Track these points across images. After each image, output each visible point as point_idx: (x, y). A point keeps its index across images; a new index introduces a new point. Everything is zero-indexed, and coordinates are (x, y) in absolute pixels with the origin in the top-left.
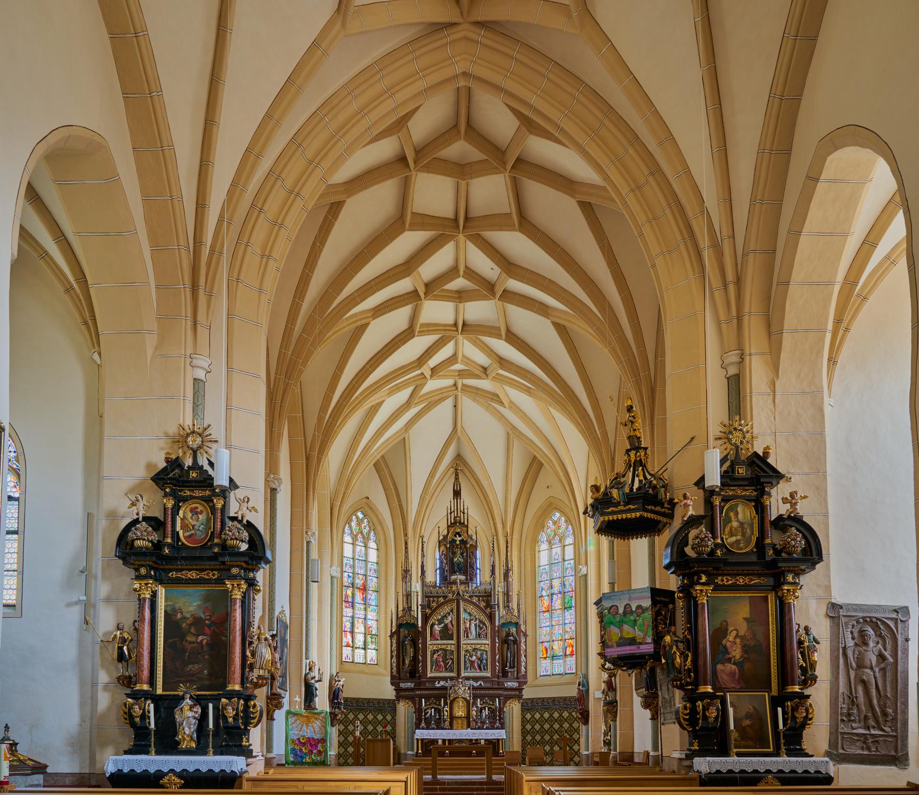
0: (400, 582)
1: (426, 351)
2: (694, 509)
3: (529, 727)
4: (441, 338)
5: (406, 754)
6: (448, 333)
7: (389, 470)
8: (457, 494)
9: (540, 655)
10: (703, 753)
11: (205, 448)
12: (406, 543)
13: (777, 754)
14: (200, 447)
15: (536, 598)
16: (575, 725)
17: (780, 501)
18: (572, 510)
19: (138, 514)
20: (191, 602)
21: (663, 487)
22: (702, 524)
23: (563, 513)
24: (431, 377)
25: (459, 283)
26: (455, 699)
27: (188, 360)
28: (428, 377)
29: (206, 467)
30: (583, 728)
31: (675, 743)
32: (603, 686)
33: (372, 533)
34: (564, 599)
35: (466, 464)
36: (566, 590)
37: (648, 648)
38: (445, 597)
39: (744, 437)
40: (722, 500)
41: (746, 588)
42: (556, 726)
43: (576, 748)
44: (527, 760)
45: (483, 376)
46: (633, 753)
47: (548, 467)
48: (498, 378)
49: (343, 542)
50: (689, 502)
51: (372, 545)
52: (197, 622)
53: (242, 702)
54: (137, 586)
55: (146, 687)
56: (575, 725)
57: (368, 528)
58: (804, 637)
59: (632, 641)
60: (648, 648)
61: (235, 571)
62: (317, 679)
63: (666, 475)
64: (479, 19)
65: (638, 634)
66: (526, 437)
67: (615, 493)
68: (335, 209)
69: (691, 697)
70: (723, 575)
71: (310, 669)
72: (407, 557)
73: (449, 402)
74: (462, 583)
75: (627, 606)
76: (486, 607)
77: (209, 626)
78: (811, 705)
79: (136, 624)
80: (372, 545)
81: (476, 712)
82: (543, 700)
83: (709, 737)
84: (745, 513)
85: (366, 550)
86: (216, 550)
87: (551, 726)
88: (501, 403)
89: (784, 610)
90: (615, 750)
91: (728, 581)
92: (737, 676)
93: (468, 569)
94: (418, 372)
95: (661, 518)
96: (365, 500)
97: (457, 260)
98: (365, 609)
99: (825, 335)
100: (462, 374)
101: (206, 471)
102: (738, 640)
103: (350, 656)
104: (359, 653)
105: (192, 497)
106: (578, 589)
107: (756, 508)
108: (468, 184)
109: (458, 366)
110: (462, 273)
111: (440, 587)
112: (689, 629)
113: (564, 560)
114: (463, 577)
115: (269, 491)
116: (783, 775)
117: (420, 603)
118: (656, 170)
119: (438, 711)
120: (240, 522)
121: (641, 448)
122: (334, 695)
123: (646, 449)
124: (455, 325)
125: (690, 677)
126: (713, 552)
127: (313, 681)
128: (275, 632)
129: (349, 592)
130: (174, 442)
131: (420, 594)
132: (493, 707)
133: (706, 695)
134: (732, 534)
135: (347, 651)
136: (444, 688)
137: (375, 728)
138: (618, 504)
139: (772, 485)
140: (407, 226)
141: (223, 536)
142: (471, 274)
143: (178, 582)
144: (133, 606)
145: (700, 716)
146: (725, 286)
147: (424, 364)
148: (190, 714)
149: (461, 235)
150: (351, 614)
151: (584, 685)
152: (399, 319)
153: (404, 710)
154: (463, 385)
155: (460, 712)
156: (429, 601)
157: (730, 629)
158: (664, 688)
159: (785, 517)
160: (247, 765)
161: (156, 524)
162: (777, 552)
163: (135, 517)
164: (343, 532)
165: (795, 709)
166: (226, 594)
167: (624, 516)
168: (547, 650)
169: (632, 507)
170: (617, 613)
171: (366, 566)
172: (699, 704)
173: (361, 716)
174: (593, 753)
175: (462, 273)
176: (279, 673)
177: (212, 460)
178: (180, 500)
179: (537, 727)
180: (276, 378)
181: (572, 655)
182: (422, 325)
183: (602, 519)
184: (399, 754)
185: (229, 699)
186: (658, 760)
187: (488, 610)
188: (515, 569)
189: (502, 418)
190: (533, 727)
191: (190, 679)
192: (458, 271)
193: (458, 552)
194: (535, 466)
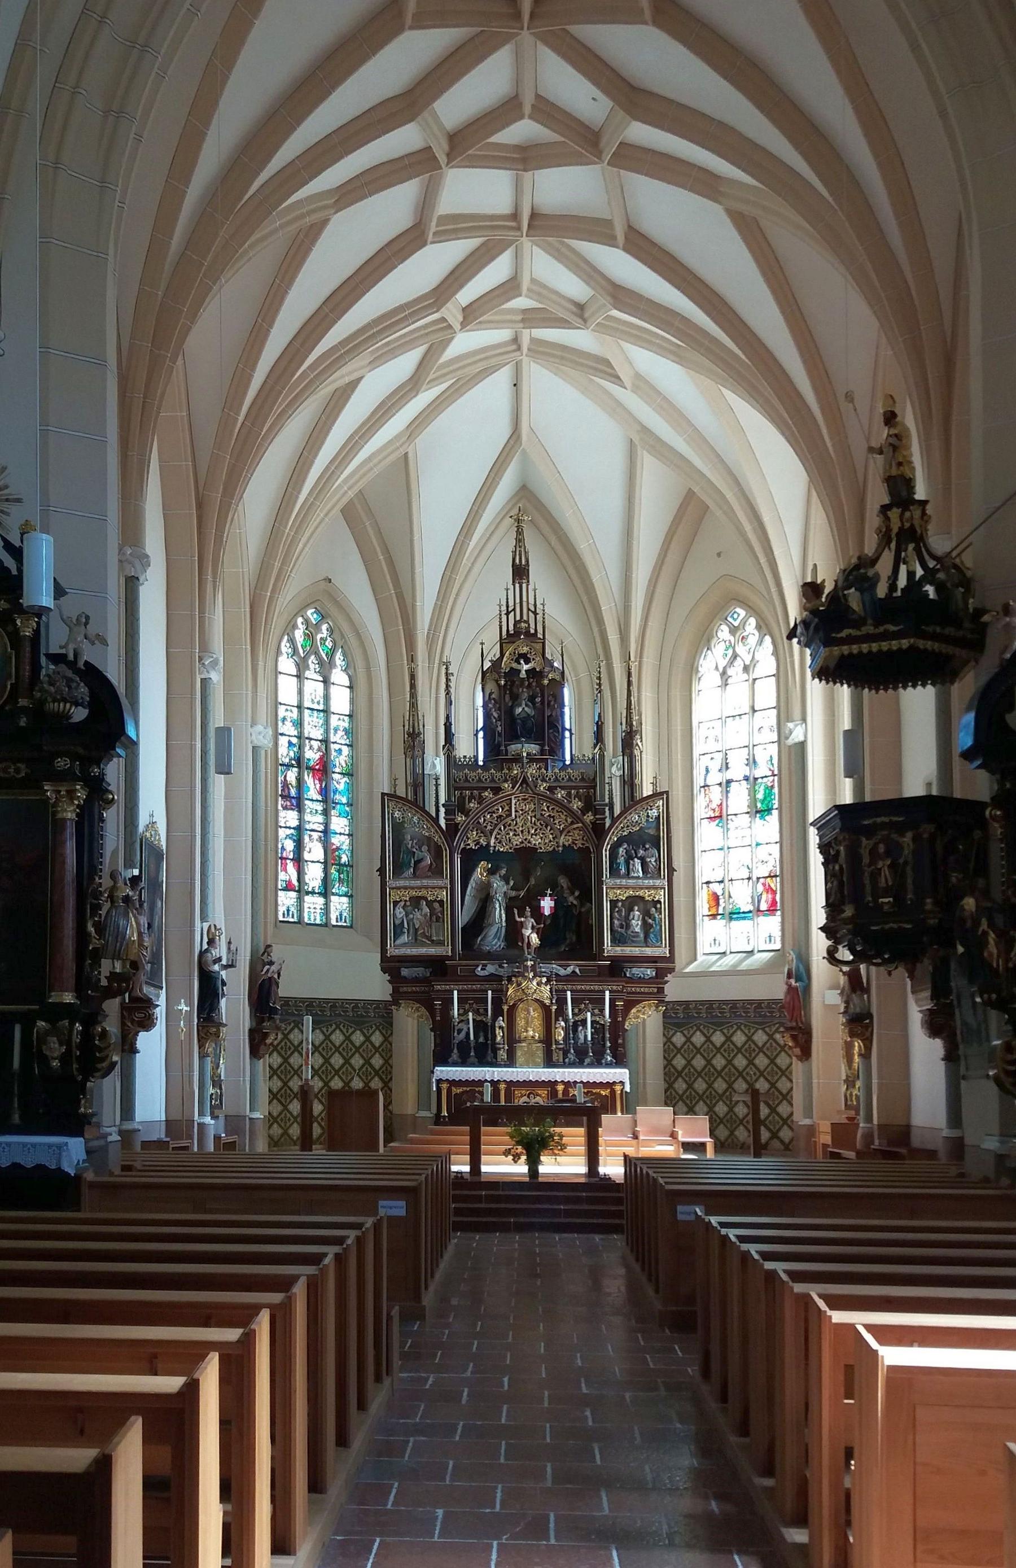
1: (452, 273)
4: (483, 244)
6: (499, 235)
8: (520, 572)
18: (771, 601)
23: (752, 610)
24: (464, 325)
25: (523, 130)
28: (457, 326)
30: (798, 1068)
32: (842, 980)
34: (752, 792)
36: (758, 773)
38: (497, 790)
42: (740, 1062)
43: (783, 1109)
45: (576, 321)
47: (719, 513)
49: (277, 673)
51: (339, 677)
53: (78, 1027)
56: (782, 1060)
57: (329, 644)
61: (62, 763)
62: (224, 962)
66: (671, 449)
67: (854, 599)
71: (211, 942)
72: (414, 705)
73: (503, 377)
74: (531, 759)
76: (584, 811)
80: (339, 677)
81: (566, 1030)
82: (710, 1005)
85: (327, 689)
86: (23, 722)
87: (730, 1062)
88: (616, 379)
90: (869, 1118)
93: (546, 729)
95: (958, 651)
96: (323, 585)
97: (518, 80)
98: (326, 813)
100: (530, 318)
104: (313, 904)
106: (785, 772)
110: (527, 109)
113: (754, 711)
114: (533, 748)
115: (122, 581)
117: (442, 800)
122: (262, 994)
123: (924, 503)
124: (515, 216)
127: (216, 967)
129: (292, 776)
131: (442, 782)
135: (286, 900)
137: (347, 1061)
138: (857, 624)
140: (409, 20)
142: (547, 111)
149: (525, 33)
150: (295, 823)
151: (800, 976)
153: (410, 1025)
155: (530, 1026)
156: (462, 798)
164: (278, 652)
166: (45, 810)
167: (875, 647)
169: (892, 628)
171: (327, 722)
175: (527, 109)
176: (147, 954)
179: (699, 1062)
181: (772, 910)
182: (444, 219)
185: (52, 1021)
187: (589, 817)
189: (617, 409)
190: (689, 1062)
192: (520, 105)
193: (523, 699)
194: (691, 515)
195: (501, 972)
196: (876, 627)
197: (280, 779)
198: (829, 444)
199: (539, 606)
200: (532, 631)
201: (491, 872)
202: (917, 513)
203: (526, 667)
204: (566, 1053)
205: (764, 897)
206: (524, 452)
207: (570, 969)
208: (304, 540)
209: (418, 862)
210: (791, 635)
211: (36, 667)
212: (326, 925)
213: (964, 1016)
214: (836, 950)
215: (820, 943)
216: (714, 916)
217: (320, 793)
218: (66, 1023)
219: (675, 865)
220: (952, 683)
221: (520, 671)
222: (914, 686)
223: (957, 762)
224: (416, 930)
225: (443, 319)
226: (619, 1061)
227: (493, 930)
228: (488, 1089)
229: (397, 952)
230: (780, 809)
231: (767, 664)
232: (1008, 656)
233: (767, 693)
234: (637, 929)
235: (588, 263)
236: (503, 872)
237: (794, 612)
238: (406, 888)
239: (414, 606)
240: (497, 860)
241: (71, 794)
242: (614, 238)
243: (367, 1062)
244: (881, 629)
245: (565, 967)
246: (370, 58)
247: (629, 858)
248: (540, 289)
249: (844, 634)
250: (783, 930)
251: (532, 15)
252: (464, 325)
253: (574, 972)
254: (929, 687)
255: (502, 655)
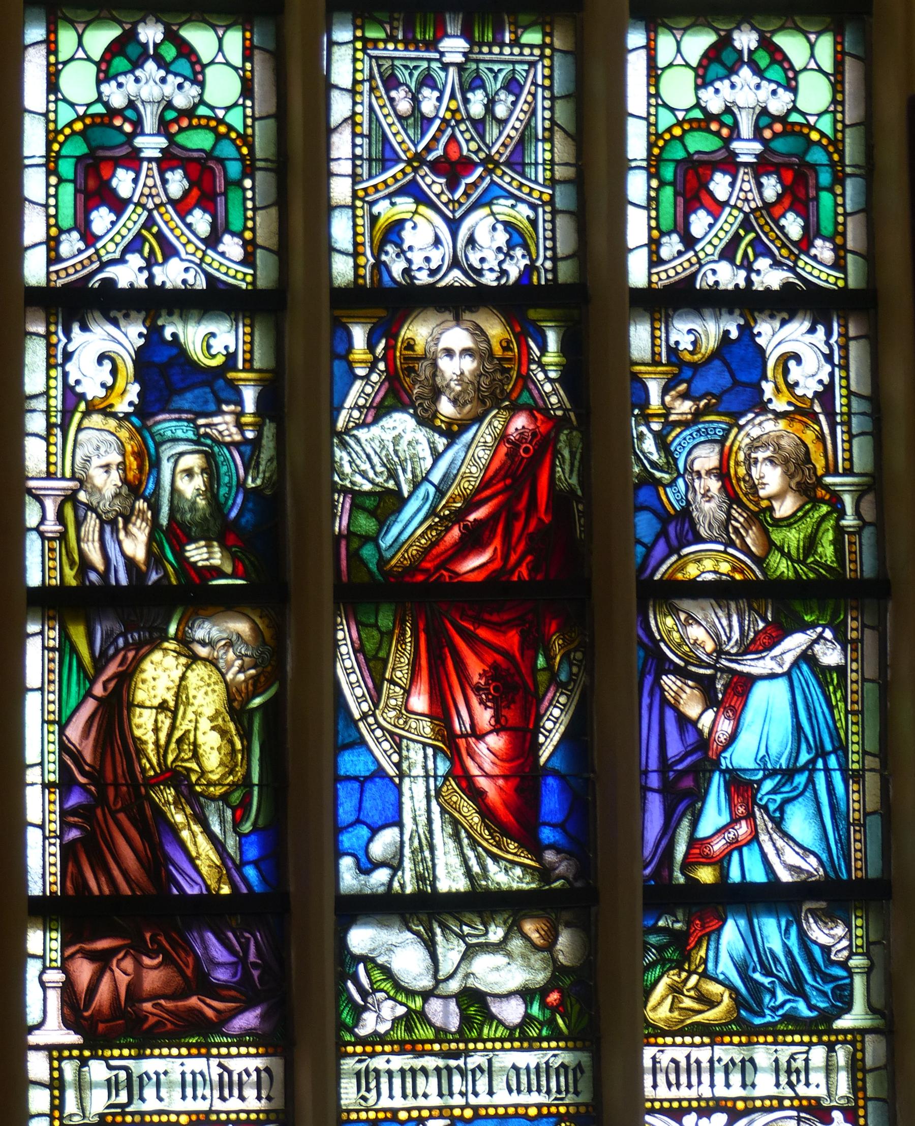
129: (186, 696)
217: (514, 821)
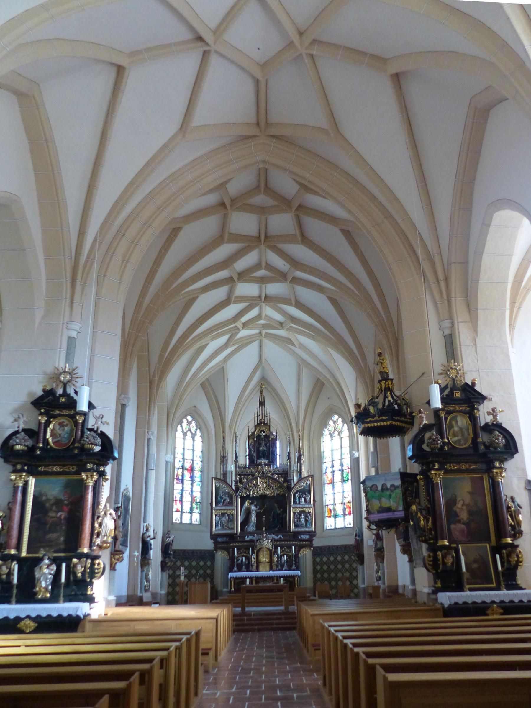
0: (219, 464)
2: (427, 420)
3: (318, 567)
5: (222, 591)
7: (212, 388)
8: (262, 404)
9: (326, 514)
10: (444, 589)
11: (73, 382)
12: (224, 438)
13: (498, 588)
14: (69, 381)
15: (321, 474)
16: (354, 565)
17: (486, 414)
18: (346, 413)
19: (18, 427)
20: (55, 488)
21: (405, 404)
22: (433, 429)
23: (340, 416)
25: (262, 273)
26: (260, 549)
27: (65, 325)
28: (241, 328)
29: (73, 394)
30: (360, 568)
31: (424, 581)
32: (374, 536)
33: (198, 430)
35: (269, 384)
37: (400, 514)
38: (253, 475)
39: (458, 373)
40: (446, 413)
41: (467, 471)
42: (340, 566)
43: (355, 582)
44: (317, 593)
45: (280, 328)
46: (397, 586)
48: (290, 329)
50: (423, 415)
52: (58, 503)
54: (13, 477)
55: (13, 552)
57: (195, 427)
58: (511, 504)
59: (388, 510)
60: (400, 514)
62: (152, 537)
63: (407, 397)
64: (272, 134)
65: (392, 504)
67: (371, 409)
68: (175, 232)
69: (433, 549)
70: (450, 463)
71: (147, 530)
72: (224, 447)
73: (256, 344)
74: (265, 465)
75: (384, 485)
76: (284, 482)
77: (67, 505)
78: (520, 552)
79: (10, 505)
80: (198, 438)
81: (277, 558)
83: (448, 577)
84: (462, 421)
86: (76, 451)
88: (294, 345)
89: (495, 487)
90: (384, 583)
91: (454, 467)
92: (466, 532)
94: (234, 325)
95: (403, 425)
98: (192, 484)
99: (505, 311)
100: (264, 326)
101: (72, 398)
102: (464, 508)
103: (179, 519)
105: (60, 415)
107: (470, 418)
108: (267, 218)
109: (262, 322)
110: (263, 266)
111: (249, 468)
112: (429, 501)
114: (266, 461)
115: (120, 406)
116: (504, 604)
118: (388, 216)
119: (248, 559)
120: (96, 432)
121: (389, 379)
122: (166, 548)
123: (392, 380)
124: (260, 297)
125: (431, 534)
126: (442, 448)
127: (148, 539)
128: (119, 505)
129: (180, 472)
130: (50, 378)
132: (290, 554)
133: (444, 547)
134: (454, 435)
136: (252, 541)
138: (373, 416)
139: (480, 404)
140: (226, 240)
141: (82, 442)
142: (269, 267)
143: (46, 473)
144: (10, 491)
145: (440, 562)
146: (438, 281)
147: (237, 321)
148: (46, 571)
151: (359, 536)
152: (220, 293)
154: (266, 333)
155: (264, 558)
157: (458, 499)
158: (414, 541)
159: (490, 424)
160: (90, 609)
161: (30, 433)
162: (487, 447)
163: (16, 429)
165: (509, 555)
167: (379, 424)
168: (331, 511)
170: (377, 490)
172: (439, 553)
173: (186, 563)
174: (368, 587)
175: (263, 266)
177: (77, 390)
178: (50, 417)
180: (129, 332)
181: (350, 514)
182: (237, 297)
183: (363, 426)
184: (217, 591)
186: (414, 592)
187: (286, 484)
188: (306, 454)
189: (294, 353)
191: (49, 545)
193: (262, 445)
194: (319, 386)
195: (254, 538)
196: (379, 417)
197: (176, 473)
198: (362, 365)
199: (268, 415)
200: (268, 424)
201: (251, 504)
202: (390, 383)
203: (263, 434)
204: (277, 566)
205: (347, 509)
206: (263, 367)
207: (279, 537)
208: (187, 394)
209: (224, 501)
210: (352, 421)
211: (83, 433)
212: (191, 524)
213: (414, 544)
214: (370, 525)
215: (365, 523)
216: (330, 517)
218: (85, 559)
219: (316, 499)
220: (405, 436)
221: (261, 436)
222: (392, 437)
223: (408, 460)
224: (223, 525)
225: (236, 326)
226: (298, 569)
227: (252, 524)
228: (248, 580)
229: (217, 532)
230: (351, 480)
231: (346, 433)
232: (421, 426)
233: (346, 442)
234: (303, 522)
235: (283, 310)
236: (255, 503)
237: (353, 414)
238: (220, 510)
239: (225, 415)
240: (253, 500)
241: (92, 476)
242: (292, 304)
243: (205, 572)
244: (381, 418)
245: (277, 536)
246: (212, 251)
247: (300, 498)
248: (268, 318)
249: (368, 420)
250: (353, 521)
251: (264, 241)
252: (243, 328)
253: (280, 537)
254: (397, 437)
255: (255, 430)
